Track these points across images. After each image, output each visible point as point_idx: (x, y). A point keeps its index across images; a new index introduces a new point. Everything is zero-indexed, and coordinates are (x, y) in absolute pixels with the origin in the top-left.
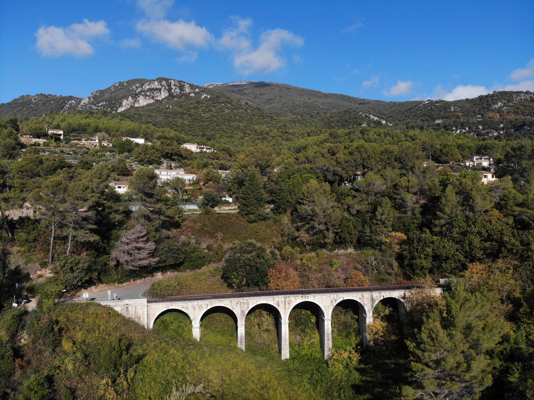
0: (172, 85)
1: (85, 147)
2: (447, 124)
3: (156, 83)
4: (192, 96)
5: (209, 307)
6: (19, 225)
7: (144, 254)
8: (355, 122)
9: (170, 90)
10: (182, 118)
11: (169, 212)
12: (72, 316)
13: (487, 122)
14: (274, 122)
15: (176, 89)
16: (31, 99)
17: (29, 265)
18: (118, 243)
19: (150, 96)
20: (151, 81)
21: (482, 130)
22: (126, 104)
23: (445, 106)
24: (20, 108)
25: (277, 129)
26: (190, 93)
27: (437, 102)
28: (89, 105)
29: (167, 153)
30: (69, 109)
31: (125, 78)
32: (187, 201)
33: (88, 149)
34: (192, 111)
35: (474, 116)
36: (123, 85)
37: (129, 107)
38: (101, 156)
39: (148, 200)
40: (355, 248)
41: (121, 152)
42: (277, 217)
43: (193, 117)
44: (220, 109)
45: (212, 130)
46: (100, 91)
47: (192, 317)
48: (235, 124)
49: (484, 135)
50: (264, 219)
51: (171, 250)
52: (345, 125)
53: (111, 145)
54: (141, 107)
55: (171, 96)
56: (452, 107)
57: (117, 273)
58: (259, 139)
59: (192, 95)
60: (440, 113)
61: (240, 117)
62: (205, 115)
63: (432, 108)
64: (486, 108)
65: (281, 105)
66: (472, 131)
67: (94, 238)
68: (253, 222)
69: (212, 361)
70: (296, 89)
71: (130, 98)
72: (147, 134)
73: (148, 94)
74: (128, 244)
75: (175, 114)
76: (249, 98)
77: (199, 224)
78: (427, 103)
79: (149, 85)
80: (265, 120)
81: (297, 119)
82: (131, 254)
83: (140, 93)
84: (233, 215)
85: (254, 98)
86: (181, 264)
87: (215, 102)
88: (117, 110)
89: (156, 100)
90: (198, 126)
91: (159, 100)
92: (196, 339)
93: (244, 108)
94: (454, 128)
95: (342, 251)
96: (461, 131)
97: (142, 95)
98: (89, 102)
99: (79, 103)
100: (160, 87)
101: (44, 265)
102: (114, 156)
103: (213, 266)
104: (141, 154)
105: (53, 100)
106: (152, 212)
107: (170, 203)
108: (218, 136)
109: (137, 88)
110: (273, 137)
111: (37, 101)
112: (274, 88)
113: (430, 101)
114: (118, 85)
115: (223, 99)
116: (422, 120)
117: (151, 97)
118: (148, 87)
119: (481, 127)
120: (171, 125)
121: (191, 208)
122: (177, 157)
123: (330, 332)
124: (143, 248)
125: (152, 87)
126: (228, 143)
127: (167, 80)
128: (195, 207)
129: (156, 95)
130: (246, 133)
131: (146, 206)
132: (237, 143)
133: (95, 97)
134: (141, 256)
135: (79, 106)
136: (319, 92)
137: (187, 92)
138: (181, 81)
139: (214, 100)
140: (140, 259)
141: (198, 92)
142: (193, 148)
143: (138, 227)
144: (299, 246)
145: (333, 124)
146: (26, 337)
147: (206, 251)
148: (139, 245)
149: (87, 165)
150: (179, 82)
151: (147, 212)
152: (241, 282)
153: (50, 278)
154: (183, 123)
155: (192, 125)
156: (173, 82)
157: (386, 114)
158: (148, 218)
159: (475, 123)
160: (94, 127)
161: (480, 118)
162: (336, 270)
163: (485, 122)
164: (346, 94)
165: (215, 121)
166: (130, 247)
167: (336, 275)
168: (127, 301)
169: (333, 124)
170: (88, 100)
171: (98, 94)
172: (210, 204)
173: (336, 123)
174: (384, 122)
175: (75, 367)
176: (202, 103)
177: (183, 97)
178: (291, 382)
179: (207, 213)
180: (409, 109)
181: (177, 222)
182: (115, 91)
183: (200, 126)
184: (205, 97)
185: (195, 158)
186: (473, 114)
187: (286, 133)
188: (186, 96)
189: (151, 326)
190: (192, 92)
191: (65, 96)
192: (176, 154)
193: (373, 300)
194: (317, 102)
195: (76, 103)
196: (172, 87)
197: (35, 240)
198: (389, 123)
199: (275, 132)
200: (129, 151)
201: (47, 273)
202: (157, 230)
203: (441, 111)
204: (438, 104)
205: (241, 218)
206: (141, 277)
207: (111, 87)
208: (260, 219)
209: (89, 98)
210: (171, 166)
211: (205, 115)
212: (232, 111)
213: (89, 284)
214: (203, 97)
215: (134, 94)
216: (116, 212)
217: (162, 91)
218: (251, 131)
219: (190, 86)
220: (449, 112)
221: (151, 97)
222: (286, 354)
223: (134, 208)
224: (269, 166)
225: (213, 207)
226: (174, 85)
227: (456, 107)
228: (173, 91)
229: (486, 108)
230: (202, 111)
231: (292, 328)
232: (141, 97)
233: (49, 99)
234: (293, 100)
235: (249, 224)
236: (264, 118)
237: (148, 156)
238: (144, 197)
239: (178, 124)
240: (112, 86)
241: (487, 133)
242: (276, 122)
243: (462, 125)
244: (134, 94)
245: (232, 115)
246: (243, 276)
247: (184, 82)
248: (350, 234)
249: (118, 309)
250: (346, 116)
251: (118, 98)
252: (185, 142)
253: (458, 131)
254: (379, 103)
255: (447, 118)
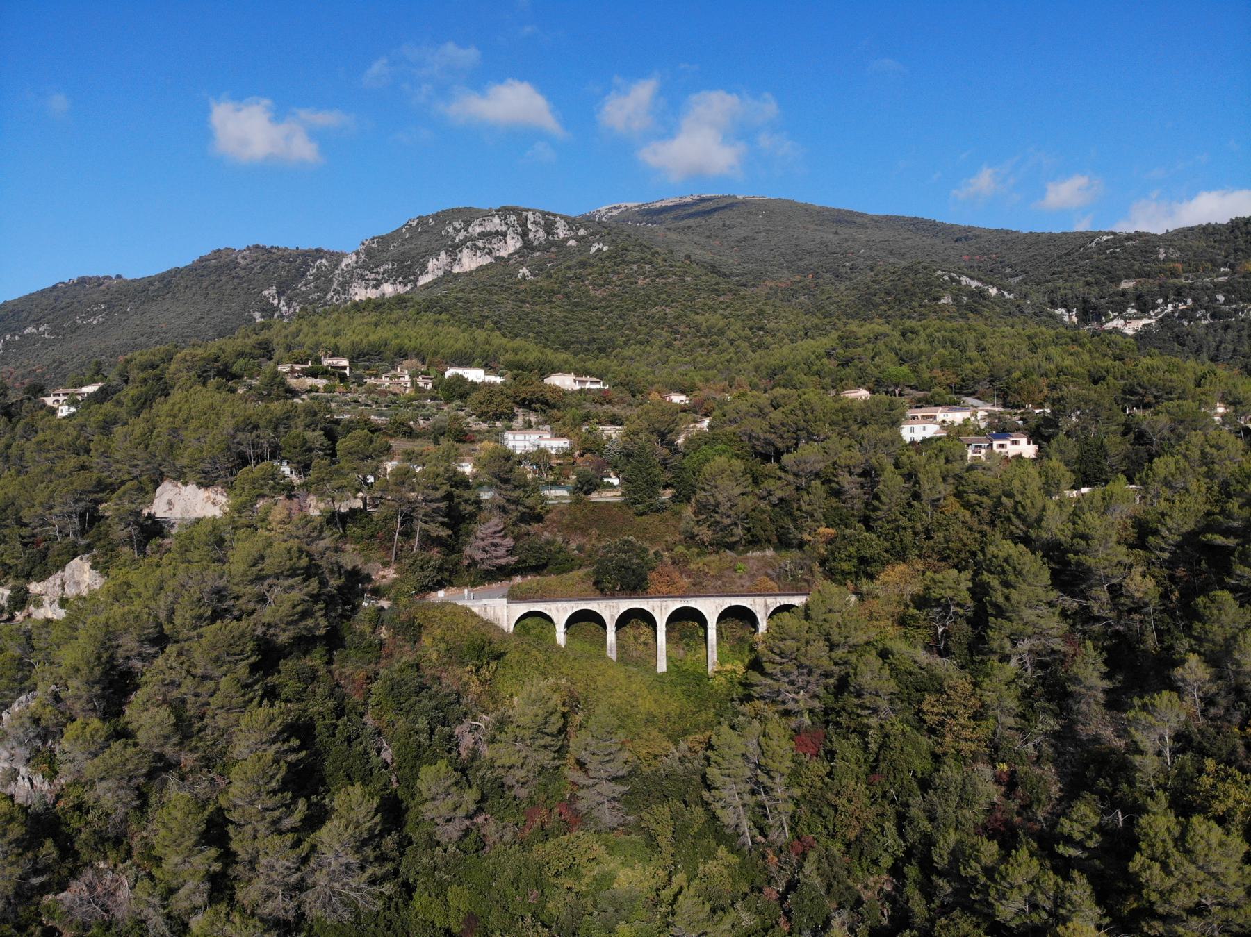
0: (529, 222)
1: (391, 392)
2: (1144, 292)
3: (496, 220)
4: (571, 246)
5: (575, 610)
6: (352, 518)
7: (502, 551)
8: (926, 294)
9: (524, 235)
10: (551, 302)
11: (530, 502)
12: (429, 614)
13: (1236, 285)
14: (738, 304)
15: (537, 231)
16: (236, 258)
17: (369, 565)
18: (472, 539)
19: (484, 249)
20: (486, 215)
21: (1224, 304)
22: (435, 267)
23: (1145, 244)
24: (214, 278)
25: (743, 320)
26: (567, 240)
27: (1129, 237)
28: (358, 271)
29: (524, 399)
30: (315, 280)
31: (429, 208)
32: (553, 484)
33: (395, 394)
34: (571, 284)
35: (1212, 270)
36: (427, 223)
37: (441, 273)
38: (418, 407)
39: (503, 486)
40: (776, 549)
41: (448, 400)
42: (677, 508)
43: (573, 300)
44: (627, 277)
45: (609, 328)
46: (379, 237)
47: (555, 621)
48: (656, 311)
49: (1228, 315)
50: (658, 510)
51: (532, 548)
52: (904, 301)
53: (430, 386)
54: (468, 274)
55: (528, 246)
56: (1162, 251)
57: (470, 575)
58: (702, 345)
59: (572, 243)
60: (1132, 265)
61: (668, 296)
62: (597, 293)
63: (1115, 252)
64: (1242, 251)
65: (767, 252)
66: (1201, 307)
67: (445, 533)
68: (642, 514)
69: (577, 665)
70: (806, 210)
71: (443, 255)
72: (488, 356)
73: (480, 244)
74: (483, 539)
75: (537, 293)
76: (696, 239)
77: (567, 517)
78: (1107, 241)
79: (481, 225)
80: (721, 299)
81: (801, 284)
82: (487, 552)
83: (463, 242)
84: (614, 504)
85: (709, 237)
86: (545, 566)
87: (618, 260)
88: (417, 280)
89: (497, 258)
90: (581, 319)
91: (503, 258)
92: (560, 645)
93: (679, 273)
94: (1160, 301)
95: (757, 554)
96: (1175, 307)
97: (468, 248)
98: (357, 263)
99: (336, 266)
100: (504, 228)
101: (386, 565)
102: (439, 408)
103: (582, 572)
104: (482, 404)
105: (282, 257)
106: (508, 500)
107: (529, 489)
108: (620, 341)
109: (457, 231)
110: (731, 342)
111: (248, 261)
112: (754, 210)
113: (1114, 234)
114: (415, 223)
115: (634, 254)
116: (1088, 284)
117: (487, 250)
118: (478, 229)
119: (1221, 298)
120: (528, 320)
121: (559, 495)
122: (539, 405)
123: (715, 640)
124: (501, 545)
125: (488, 229)
126: (638, 358)
127: (518, 212)
128: (564, 493)
129: (495, 246)
130: (677, 333)
131: (500, 494)
132: (655, 357)
133: (369, 252)
134: (498, 554)
135: (337, 272)
136: (862, 215)
137: (562, 236)
138: (549, 214)
139: (615, 258)
140: (496, 558)
141: (583, 237)
142: (564, 382)
143: (496, 520)
144: (698, 546)
145: (876, 299)
146: (385, 632)
147: (576, 552)
148: (497, 541)
149: (859, 695)
150: (545, 214)
151: (503, 502)
152: (614, 587)
153: (396, 579)
154: (551, 316)
155: (570, 318)
156: (530, 217)
157: (1016, 265)
158: (503, 510)
159: (1208, 289)
160: (396, 349)
161: (1225, 275)
162: (741, 577)
163: (1231, 285)
164: (927, 218)
165: (617, 307)
166: (487, 542)
167: (739, 582)
168: (485, 601)
169: (876, 299)
170: (354, 257)
171: (375, 245)
172: (585, 488)
173: (883, 295)
174: (993, 291)
175: (438, 657)
176: (590, 265)
177: (553, 249)
178: (662, 691)
179: (578, 501)
180: (1066, 255)
181: (539, 514)
182: (411, 238)
183: (585, 320)
184: (599, 250)
185: (569, 405)
186: (1209, 266)
187: (760, 329)
188: (559, 246)
189: (511, 629)
190: (572, 238)
191: (307, 248)
192: (538, 401)
193: (766, 606)
194: (854, 240)
195: (330, 266)
196: (529, 227)
197: (371, 537)
198: (1005, 293)
199: (737, 329)
200: (463, 396)
201: (391, 574)
202: (515, 525)
203: (1134, 259)
204: (1130, 243)
205: (625, 508)
206: (497, 580)
207: (401, 229)
208: (652, 511)
209: (357, 253)
210: (530, 421)
211: (597, 293)
212: (653, 281)
213: (440, 585)
214: (593, 250)
215: (450, 246)
216: (466, 501)
217: (508, 238)
218: (689, 326)
219: (568, 223)
220: (1153, 261)
221: (487, 250)
222: (662, 666)
223: (486, 495)
224: (671, 431)
225: (588, 493)
226: (534, 222)
227: (1171, 250)
228: (531, 235)
229: (1242, 251)
230: (591, 284)
231: (669, 639)
232: (465, 251)
233: (275, 256)
234: (798, 238)
235: (637, 518)
236: (720, 296)
237: (493, 407)
238: (499, 484)
239: (543, 318)
240: (404, 226)
241: (1236, 310)
242: (744, 303)
243: (1179, 294)
244: (450, 246)
245: (653, 291)
246: (617, 580)
247: (555, 216)
248: (765, 531)
249: (475, 610)
250: (907, 279)
251: (418, 254)
252: (555, 370)
253: (1170, 308)
254: (1007, 239)
255: (1148, 275)
